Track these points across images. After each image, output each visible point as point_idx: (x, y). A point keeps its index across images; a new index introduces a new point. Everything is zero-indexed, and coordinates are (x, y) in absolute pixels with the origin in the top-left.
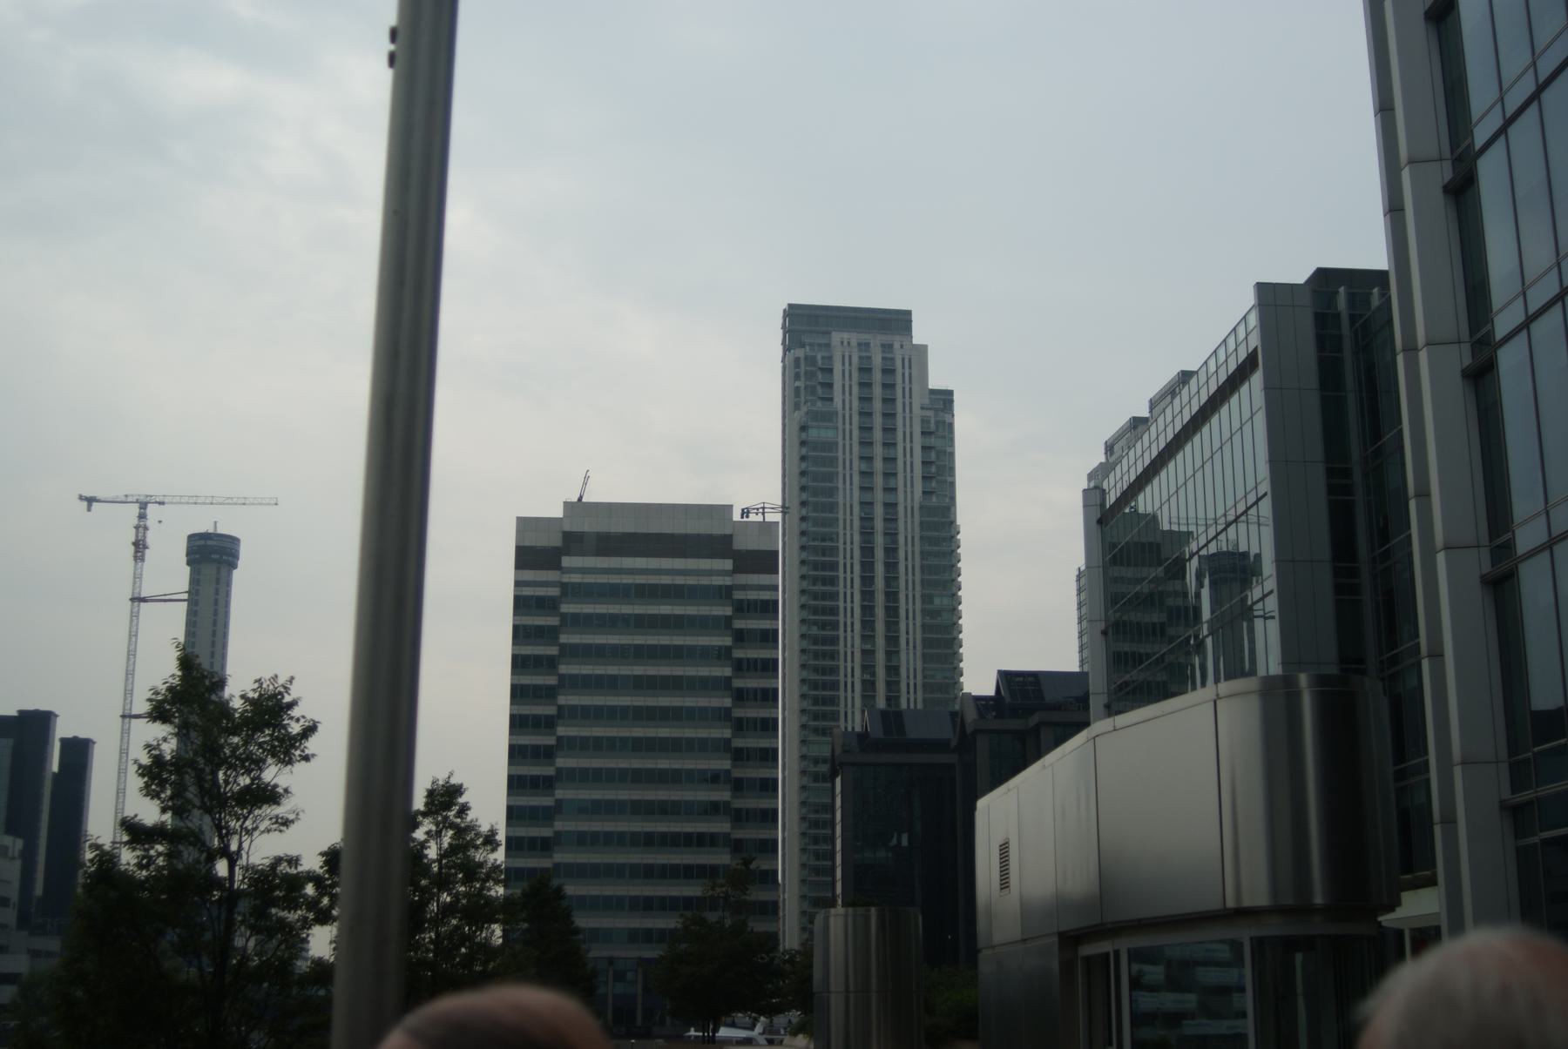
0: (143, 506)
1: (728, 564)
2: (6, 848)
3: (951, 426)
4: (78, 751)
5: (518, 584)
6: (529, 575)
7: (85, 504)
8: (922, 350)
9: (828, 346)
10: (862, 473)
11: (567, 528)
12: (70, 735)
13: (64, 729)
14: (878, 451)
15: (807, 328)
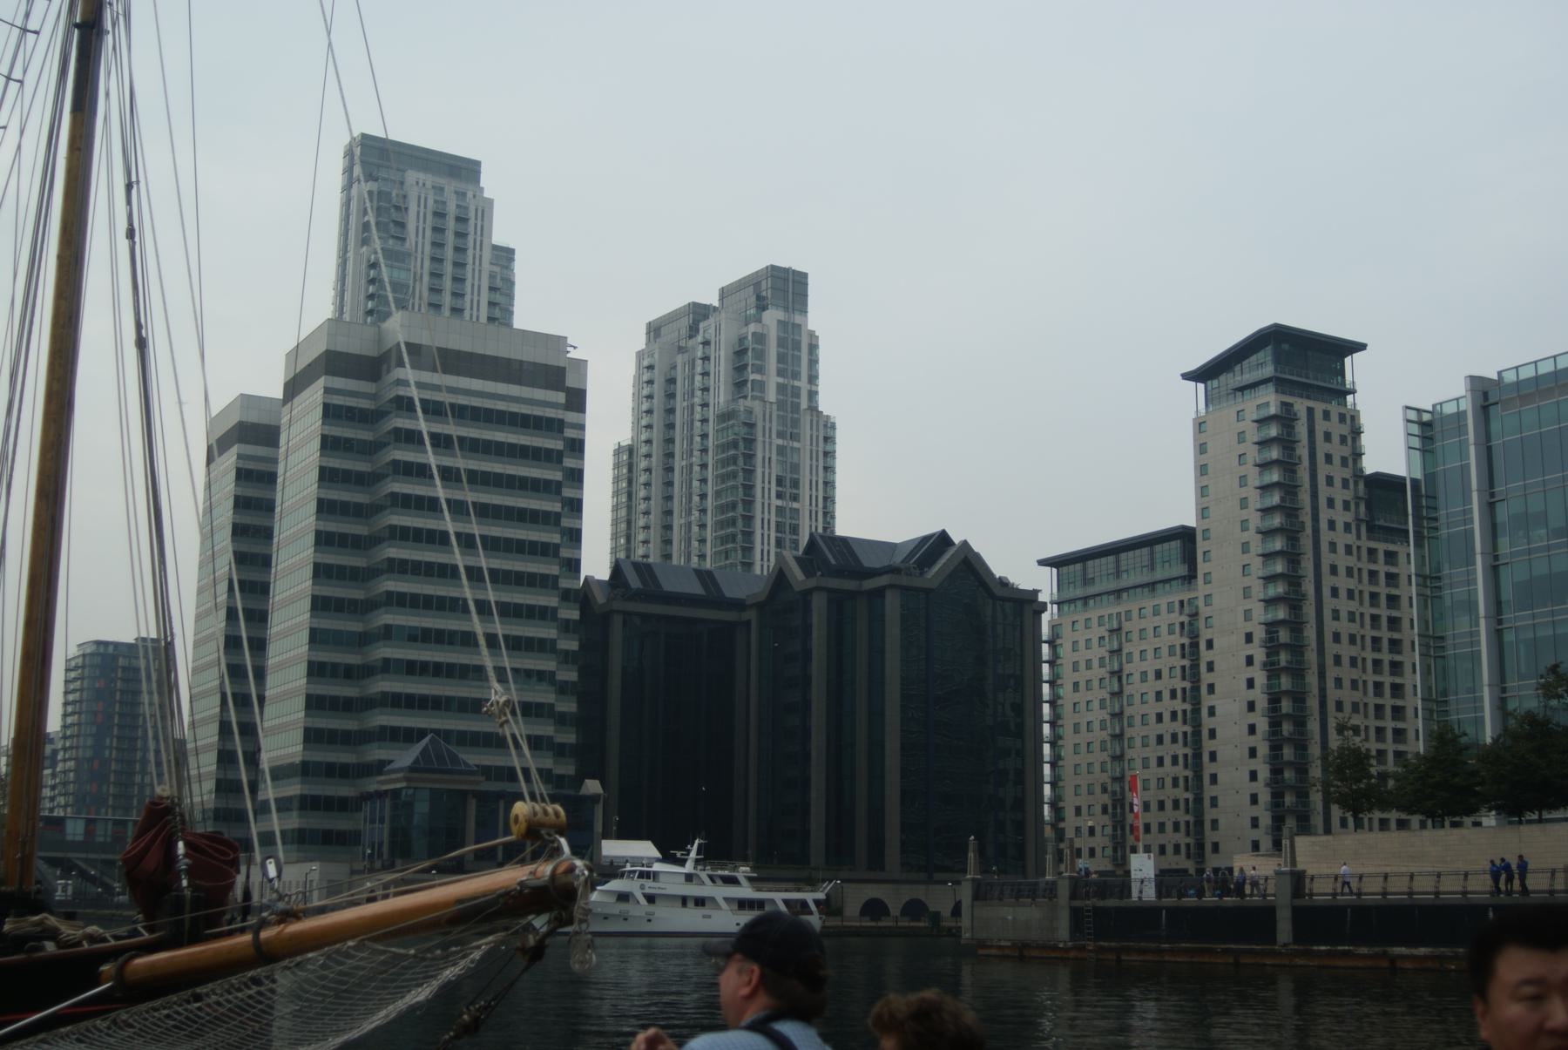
1: (561, 397)
15: (378, 163)
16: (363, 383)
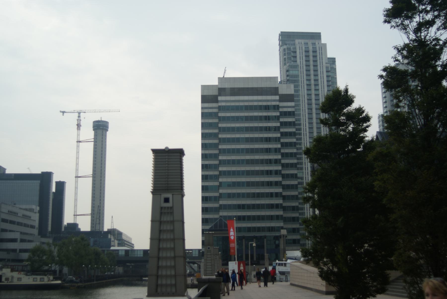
0: (79, 113)
2: (33, 209)
3: (335, 69)
4: (61, 185)
5: (202, 108)
6: (206, 105)
7: (62, 113)
8: (325, 45)
9: (294, 44)
10: (307, 85)
11: (220, 87)
12: (58, 180)
13: (55, 179)
14: (312, 77)
15: (287, 38)
16: (214, 104)
